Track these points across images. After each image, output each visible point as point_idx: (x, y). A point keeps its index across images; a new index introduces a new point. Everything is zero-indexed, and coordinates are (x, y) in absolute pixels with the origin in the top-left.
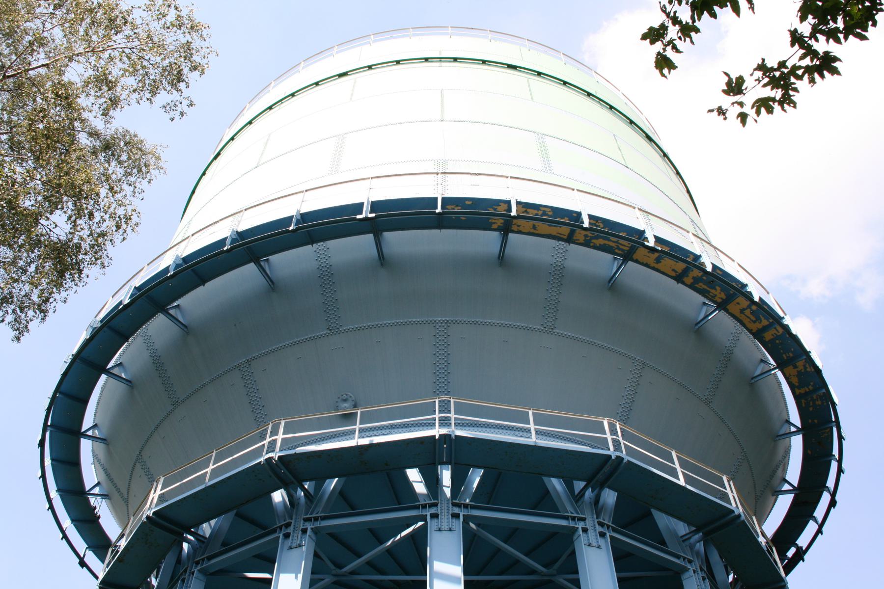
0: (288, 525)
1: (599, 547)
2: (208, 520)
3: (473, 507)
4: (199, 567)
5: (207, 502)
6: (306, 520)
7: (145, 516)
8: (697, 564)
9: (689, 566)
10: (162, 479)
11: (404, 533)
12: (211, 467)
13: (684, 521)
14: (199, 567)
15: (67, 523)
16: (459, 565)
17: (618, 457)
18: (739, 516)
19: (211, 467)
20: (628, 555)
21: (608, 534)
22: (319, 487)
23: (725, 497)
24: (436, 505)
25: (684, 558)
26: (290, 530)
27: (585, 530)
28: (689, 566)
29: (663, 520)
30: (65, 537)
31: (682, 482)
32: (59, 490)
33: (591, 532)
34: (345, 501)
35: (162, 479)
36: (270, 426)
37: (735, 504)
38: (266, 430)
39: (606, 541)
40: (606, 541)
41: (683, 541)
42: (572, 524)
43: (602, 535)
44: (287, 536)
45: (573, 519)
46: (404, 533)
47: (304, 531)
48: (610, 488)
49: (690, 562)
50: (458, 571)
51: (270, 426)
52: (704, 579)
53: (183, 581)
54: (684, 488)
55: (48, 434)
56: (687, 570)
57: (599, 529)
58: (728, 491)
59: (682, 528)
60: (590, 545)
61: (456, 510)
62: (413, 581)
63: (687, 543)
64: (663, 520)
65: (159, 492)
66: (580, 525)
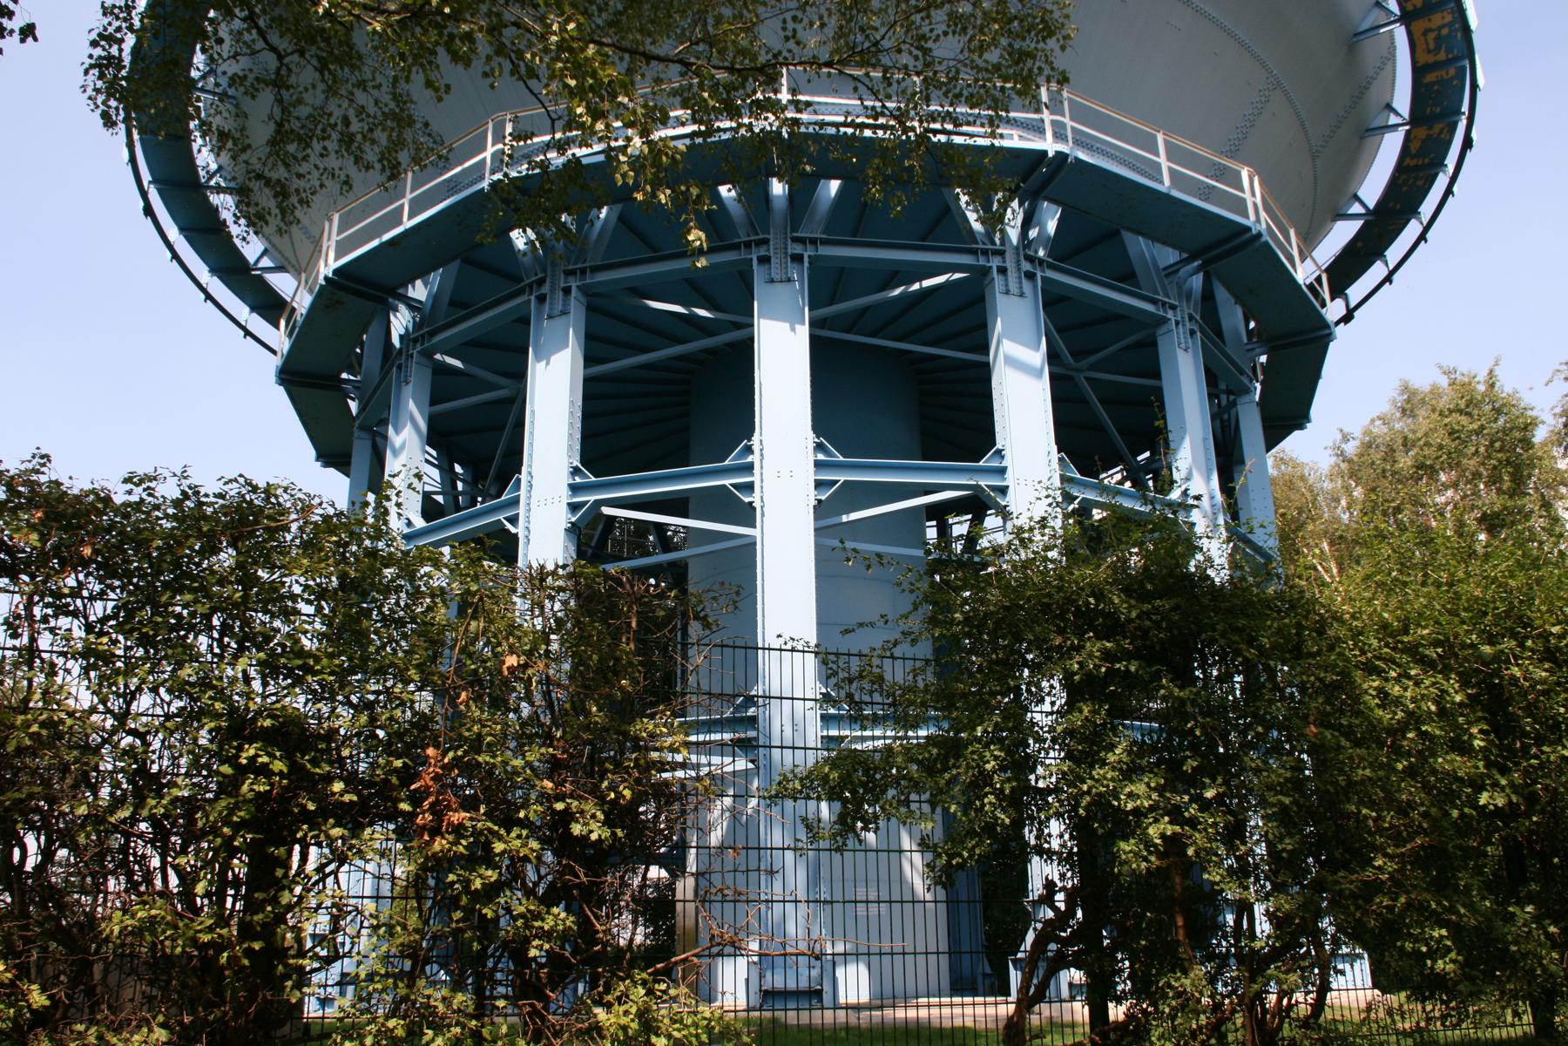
0: (541, 282)
1: (1022, 295)
2: (422, 274)
3: (825, 242)
4: (419, 348)
5: (412, 255)
6: (569, 273)
7: (321, 277)
8: (1185, 310)
9: (1170, 315)
10: (336, 218)
11: (927, 283)
12: (409, 196)
13: (1174, 247)
14: (419, 348)
15: (173, 233)
16: (1038, 349)
17: (1058, 153)
18: (1259, 235)
19: (409, 196)
20: (1062, 299)
21: (1039, 274)
22: (584, 220)
23: (1240, 207)
24: (766, 242)
25: (1164, 304)
26: (546, 289)
27: (1002, 271)
28: (1170, 315)
29: (1140, 247)
30: (209, 297)
31: (1166, 185)
32: (182, 229)
33: (1012, 275)
34: (853, 218)
35: (336, 218)
36: (490, 125)
37: (1257, 218)
38: (486, 132)
39: (1035, 287)
40: (1035, 287)
41: (1167, 276)
42: (982, 261)
43: (1030, 276)
44: (541, 299)
45: (985, 253)
46: (927, 283)
47: (567, 291)
48: (1052, 201)
49: (1173, 308)
50: (1037, 357)
51: (490, 125)
52: (1192, 333)
53: (399, 367)
54: (1167, 198)
55: (135, 132)
56: (1165, 320)
57: (1026, 266)
58: (1247, 195)
59: (1169, 256)
60: (1007, 292)
61: (798, 249)
62: (707, 351)
63: (1175, 278)
64: (1140, 247)
65: (335, 237)
66: (995, 262)
